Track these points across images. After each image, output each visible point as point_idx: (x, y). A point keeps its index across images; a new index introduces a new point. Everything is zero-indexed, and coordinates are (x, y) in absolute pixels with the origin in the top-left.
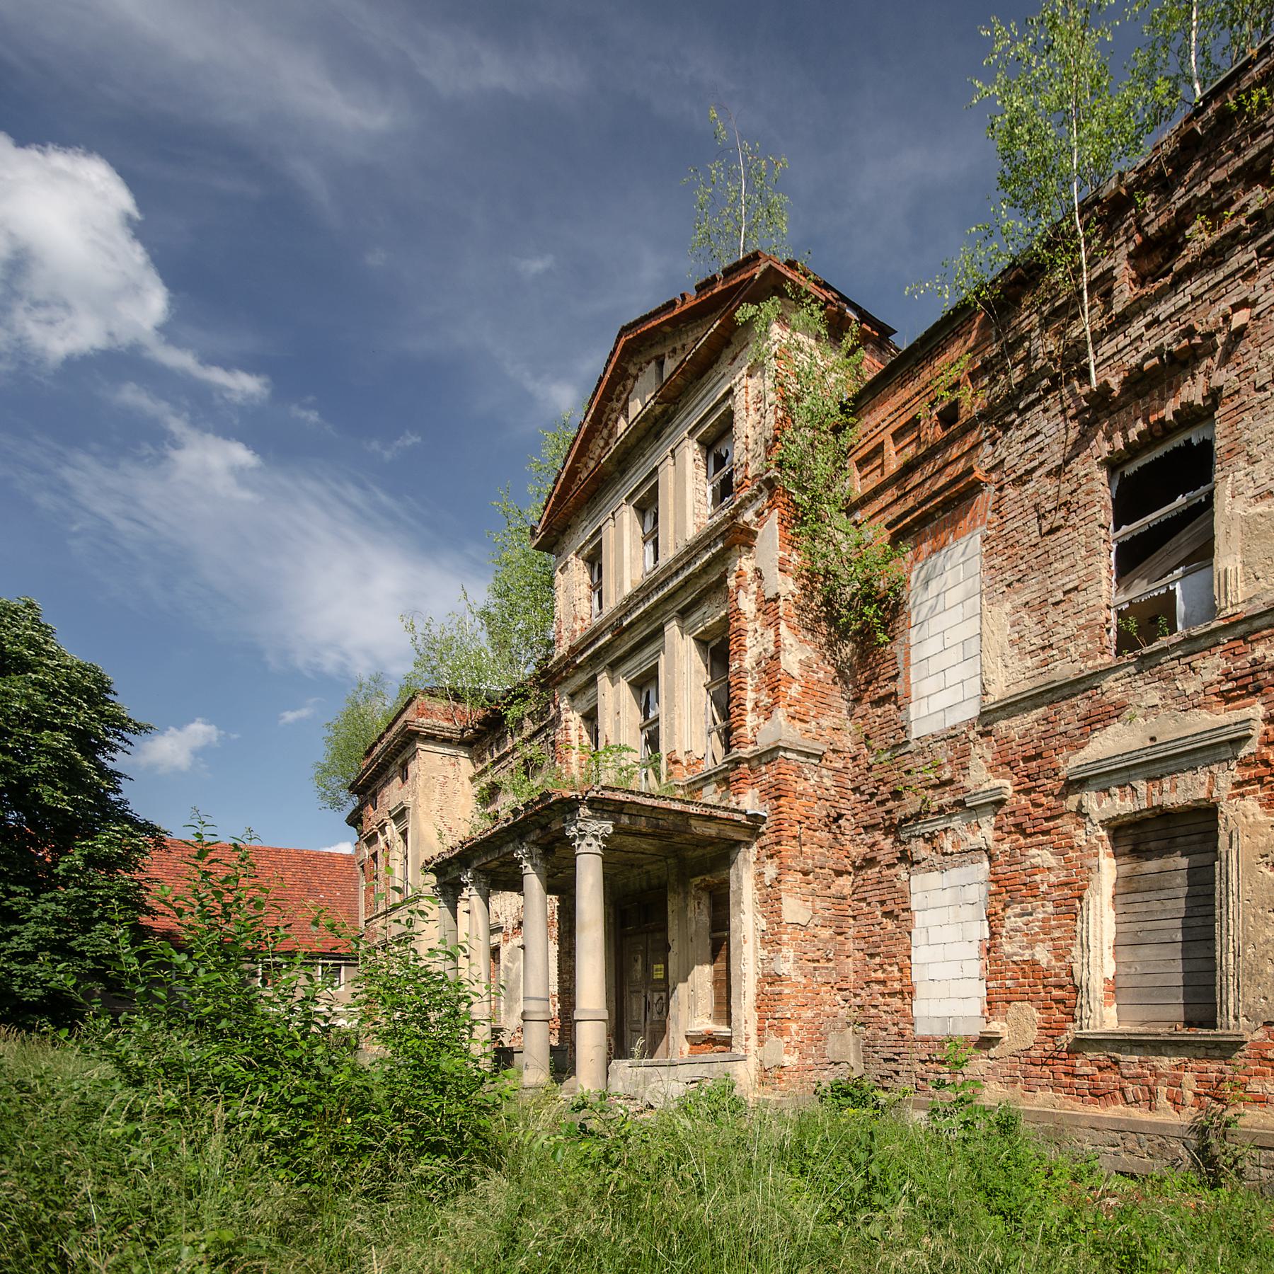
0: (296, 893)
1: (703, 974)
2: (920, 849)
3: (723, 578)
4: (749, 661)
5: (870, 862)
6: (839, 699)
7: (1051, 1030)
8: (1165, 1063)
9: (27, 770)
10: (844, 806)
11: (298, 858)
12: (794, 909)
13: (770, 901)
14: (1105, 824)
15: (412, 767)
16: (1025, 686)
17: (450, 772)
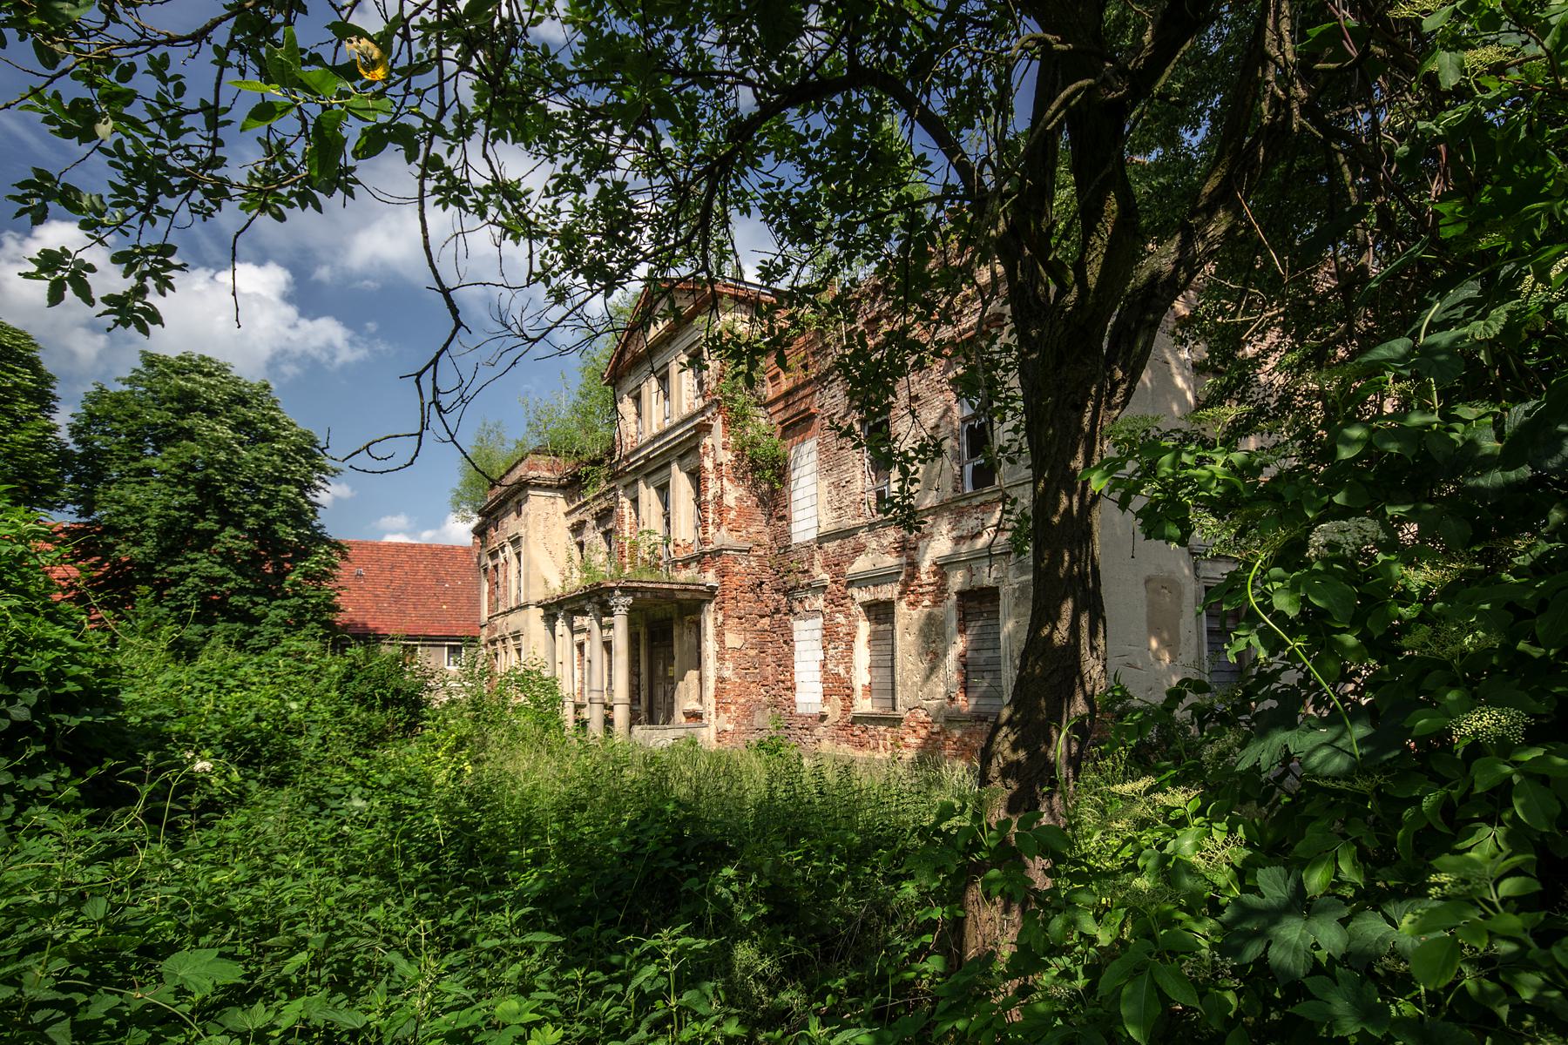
0: (427, 582)
1: (692, 675)
2: (797, 607)
3: (697, 447)
4: (709, 497)
5: (777, 611)
6: (759, 515)
7: (846, 710)
8: (881, 729)
9: (271, 514)
10: (764, 577)
11: (428, 552)
12: (732, 640)
13: (720, 635)
14: (862, 604)
15: (525, 508)
16: (832, 527)
17: (550, 509)
